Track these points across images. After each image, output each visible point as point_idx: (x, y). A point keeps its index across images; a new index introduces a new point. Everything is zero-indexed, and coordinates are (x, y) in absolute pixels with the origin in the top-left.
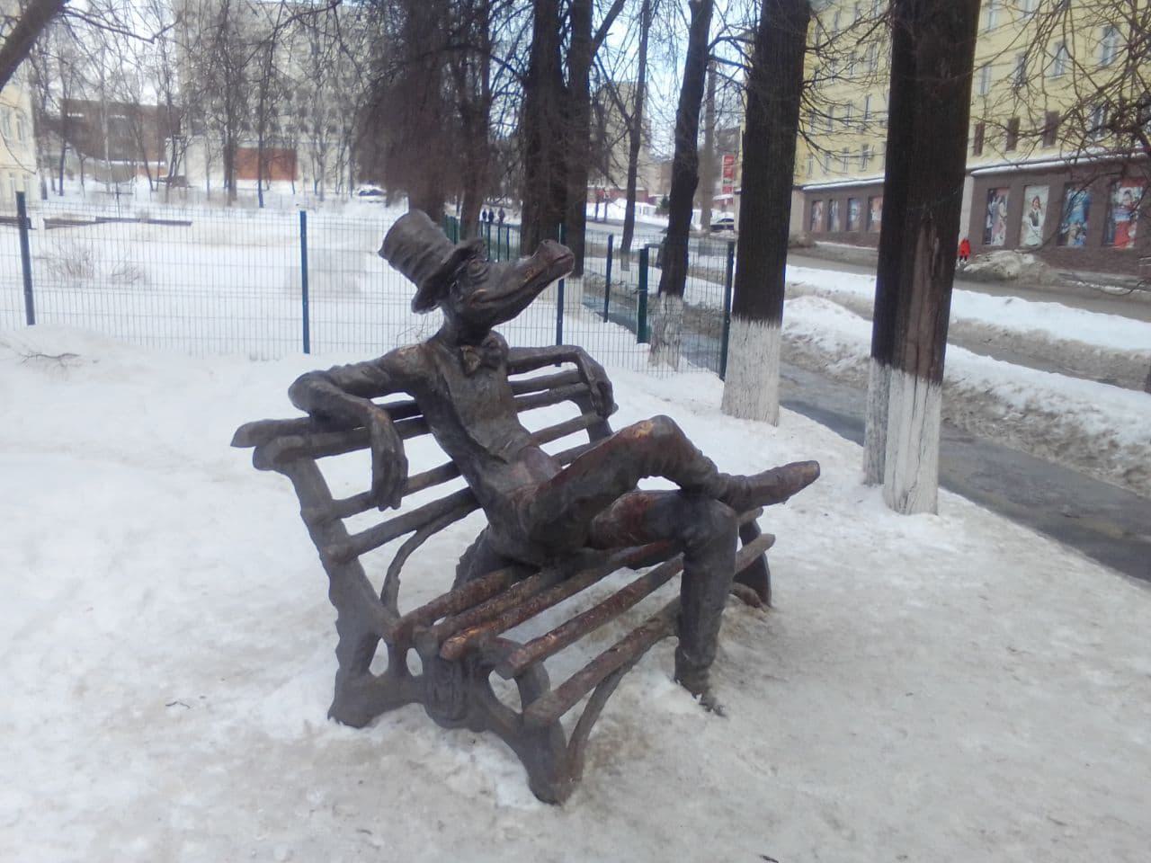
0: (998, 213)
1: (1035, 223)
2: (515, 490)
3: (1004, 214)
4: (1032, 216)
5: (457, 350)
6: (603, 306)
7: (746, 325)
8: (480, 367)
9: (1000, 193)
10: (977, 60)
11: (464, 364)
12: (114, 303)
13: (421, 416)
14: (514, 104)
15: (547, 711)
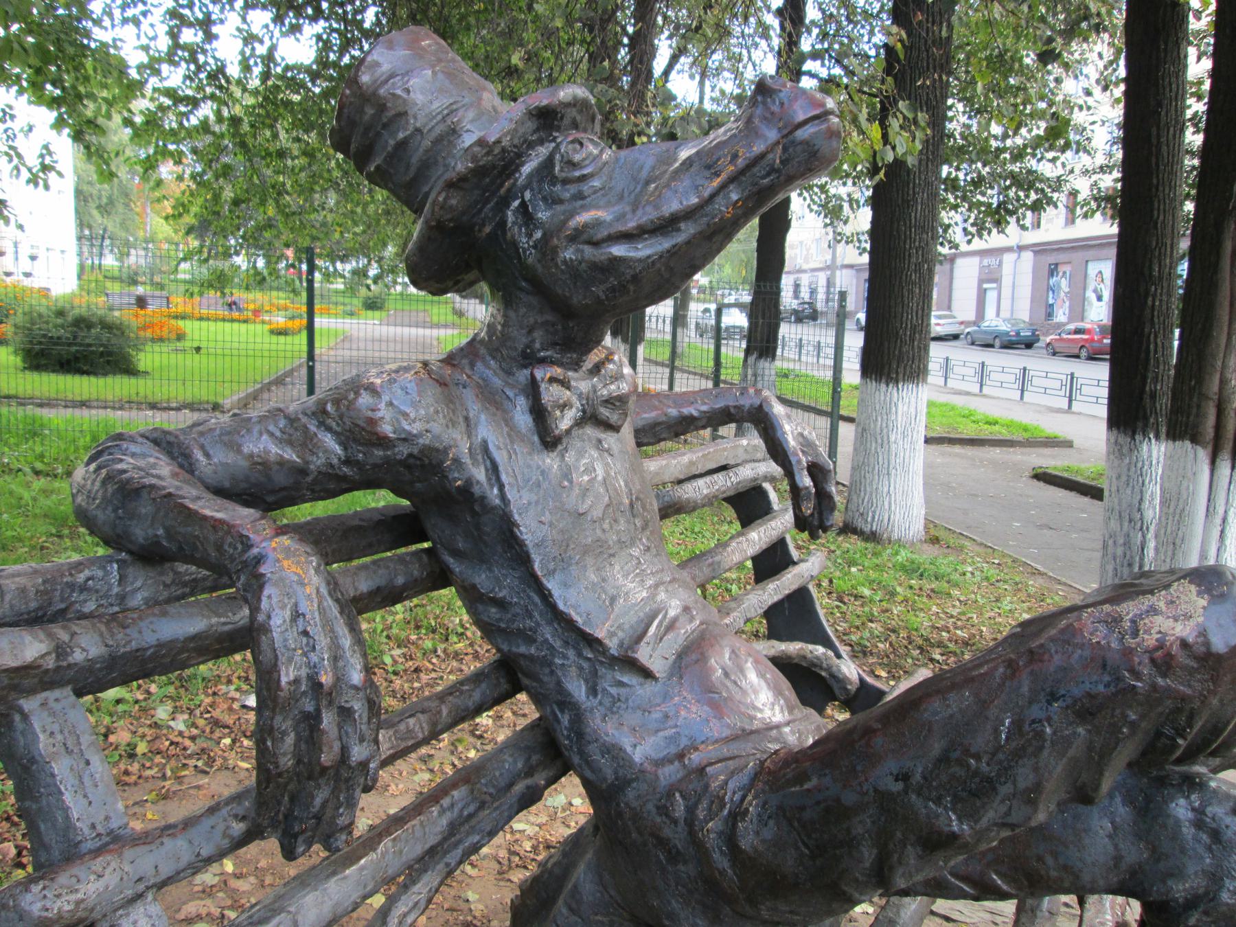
0: (1059, 287)
1: (1099, 298)
2: (681, 756)
3: (1067, 290)
4: (1095, 291)
5: (523, 375)
6: (666, 381)
7: (883, 386)
8: (579, 423)
9: (1061, 269)
10: (789, 273)
11: (539, 413)
12: (120, 405)
13: (426, 545)
14: (371, 647)
15: (497, 678)
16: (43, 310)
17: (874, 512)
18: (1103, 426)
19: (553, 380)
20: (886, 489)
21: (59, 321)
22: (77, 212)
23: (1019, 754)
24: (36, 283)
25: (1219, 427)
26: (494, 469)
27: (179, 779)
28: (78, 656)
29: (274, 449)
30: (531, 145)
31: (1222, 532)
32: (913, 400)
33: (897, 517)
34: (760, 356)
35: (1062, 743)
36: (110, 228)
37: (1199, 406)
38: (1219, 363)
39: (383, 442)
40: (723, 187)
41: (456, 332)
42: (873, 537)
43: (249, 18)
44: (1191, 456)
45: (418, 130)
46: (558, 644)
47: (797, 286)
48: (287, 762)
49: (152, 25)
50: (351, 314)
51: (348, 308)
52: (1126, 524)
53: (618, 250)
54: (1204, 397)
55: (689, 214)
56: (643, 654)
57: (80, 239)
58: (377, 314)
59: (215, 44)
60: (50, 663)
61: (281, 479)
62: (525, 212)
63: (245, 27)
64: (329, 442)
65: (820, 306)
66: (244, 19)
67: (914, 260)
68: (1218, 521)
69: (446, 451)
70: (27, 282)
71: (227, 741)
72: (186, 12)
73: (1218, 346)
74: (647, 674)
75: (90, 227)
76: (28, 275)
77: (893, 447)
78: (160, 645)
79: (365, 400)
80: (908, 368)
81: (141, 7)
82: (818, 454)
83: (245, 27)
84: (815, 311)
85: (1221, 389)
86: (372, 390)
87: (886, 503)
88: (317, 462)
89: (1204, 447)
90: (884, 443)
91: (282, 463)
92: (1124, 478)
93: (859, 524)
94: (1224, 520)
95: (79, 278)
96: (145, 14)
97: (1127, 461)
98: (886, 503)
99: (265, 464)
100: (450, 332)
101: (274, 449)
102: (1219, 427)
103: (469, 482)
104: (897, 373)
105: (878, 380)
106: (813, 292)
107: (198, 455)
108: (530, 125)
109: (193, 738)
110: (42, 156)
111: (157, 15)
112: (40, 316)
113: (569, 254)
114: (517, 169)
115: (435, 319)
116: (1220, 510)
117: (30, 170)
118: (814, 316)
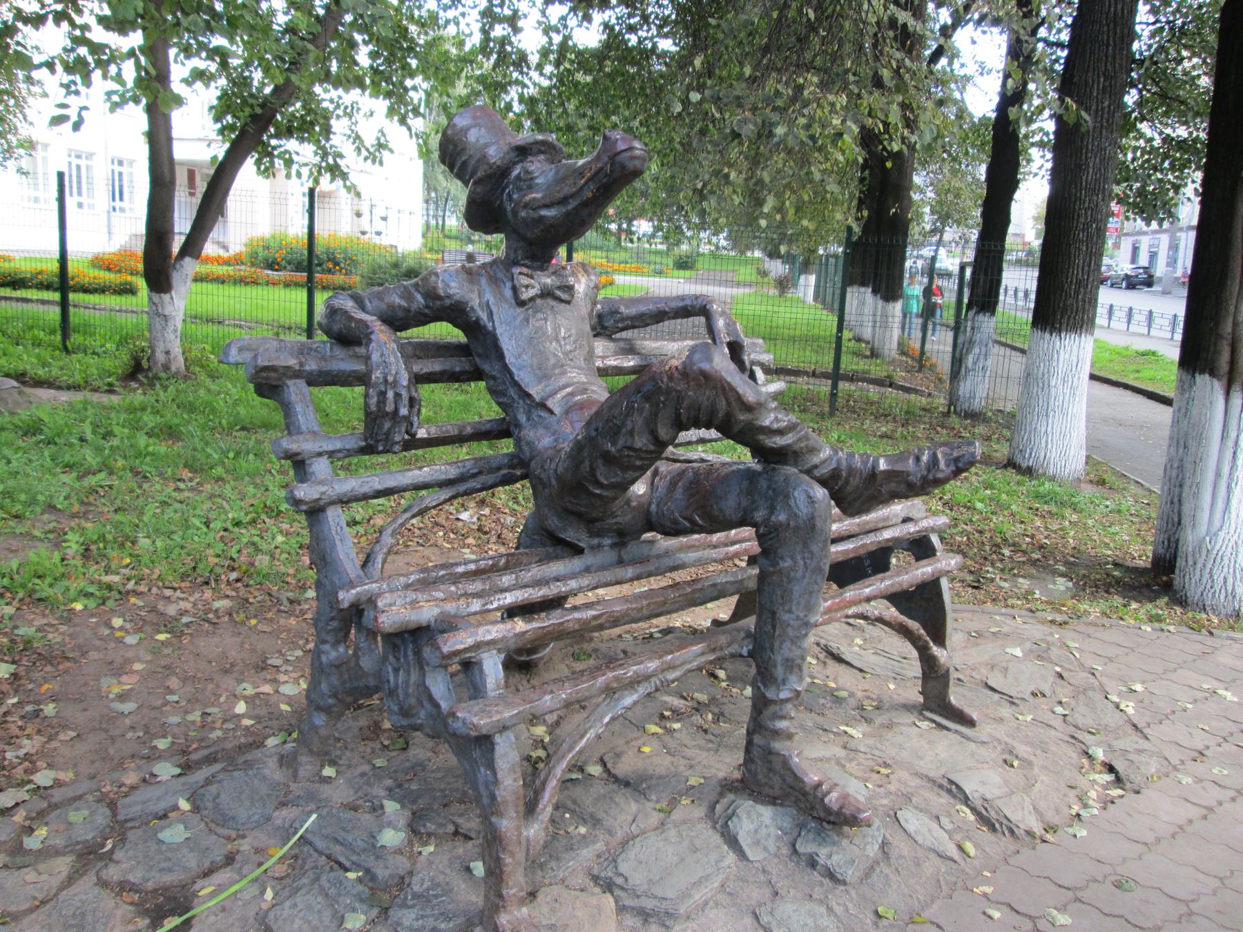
16: (382, 262)
17: (1032, 449)
18: (1175, 368)
19: (520, 273)
20: (1043, 429)
21: (394, 272)
22: (425, 176)
23: (627, 415)
24: (385, 241)
25: (1233, 362)
26: (491, 314)
27: (407, 546)
28: (307, 368)
29: (397, 300)
30: (516, 163)
31: (1235, 453)
32: (1075, 349)
33: (1053, 454)
34: (977, 313)
35: (641, 410)
36: (453, 192)
37: (1215, 345)
38: (1232, 308)
39: (439, 298)
40: (586, 183)
41: (753, 290)
42: (1029, 472)
43: (548, 12)
44: (1209, 387)
45: (471, 156)
46: (516, 397)
47: (1135, 250)
48: (373, 408)
49: (468, 25)
50: (659, 273)
51: (658, 267)
52: (1181, 450)
53: (544, 212)
54: (1219, 337)
55: (572, 196)
56: (550, 403)
57: (427, 202)
58: (688, 273)
59: (519, 36)
60: (297, 367)
61: (400, 314)
62: (509, 195)
63: (544, 20)
64: (419, 297)
65: (1160, 270)
66: (543, 13)
67: (1082, 220)
68: (1230, 443)
69: (467, 303)
70: (377, 240)
71: (441, 534)
72: (498, 10)
73: (1231, 292)
74: (551, 412)
75: (436, 190)
76: (379, 233)
77: (1053, 391)
78: (340, 371)
79: (433, 278)
80: (1072, 320)
81: (461, 9)
82: (738, 335)
83: (544, 20)
84: (1151, 276)
85: (1234, 330)
86: (436, 274)
87: (1043, 442)
88: (414, 307)
89: (1219, 380)
90: (1046, 387)
91: (400, 306)
92: (1183, 411)
93: (1018, 459)
94: (1236, 443)
95: (424, 236)
96: (463, 15)
97: (1187, 395)
98: (1043, 442)
99: (393, 307)
100: (747, 290)
101: (397, 300)
102: (1233, 362)
103: (478, 319)
104: (1061, 324)
105: (1043, 329)
106: (1153, 256)
107: (367, 302)
108: (512, 155)
109: (420, 529)
110: (378, 139)
111: (474, 15)
112: (380, 267)
113: (523, 214)
114: (509, 174)
115: (741, 278)
116: (1233, 435)
117: (367, 150)
118: (1149, 282)
